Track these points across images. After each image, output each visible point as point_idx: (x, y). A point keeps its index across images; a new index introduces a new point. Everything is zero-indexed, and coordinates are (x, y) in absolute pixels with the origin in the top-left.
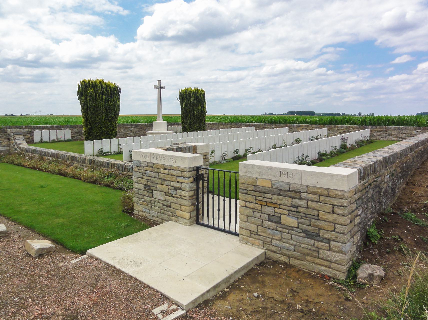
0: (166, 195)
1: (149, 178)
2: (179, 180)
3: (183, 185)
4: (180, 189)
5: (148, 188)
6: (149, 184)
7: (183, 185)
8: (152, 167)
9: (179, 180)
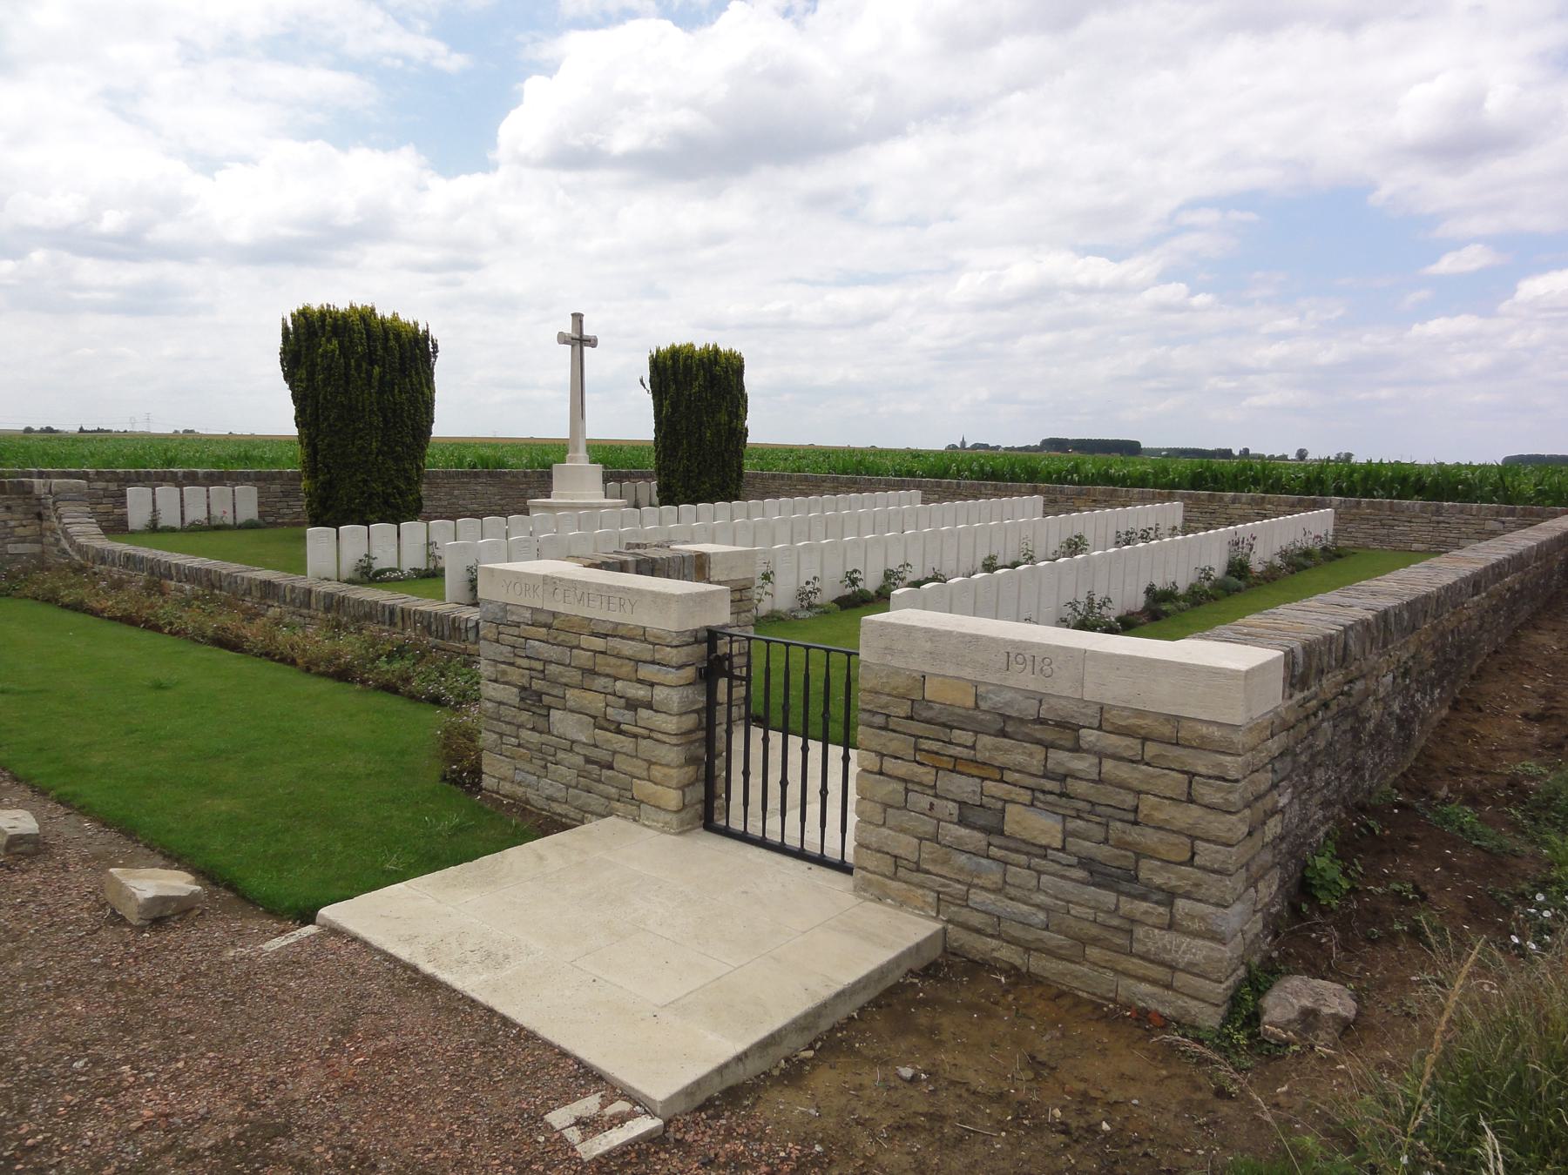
0: (597, 726)
1: (539, 666)
2: (646, 672)
3: (660, 693)
4: (649, 706)
5: (534, 700)
6: (537, 685)
7: (660, 693)
8: (549, 626)
9: (646, 672)
